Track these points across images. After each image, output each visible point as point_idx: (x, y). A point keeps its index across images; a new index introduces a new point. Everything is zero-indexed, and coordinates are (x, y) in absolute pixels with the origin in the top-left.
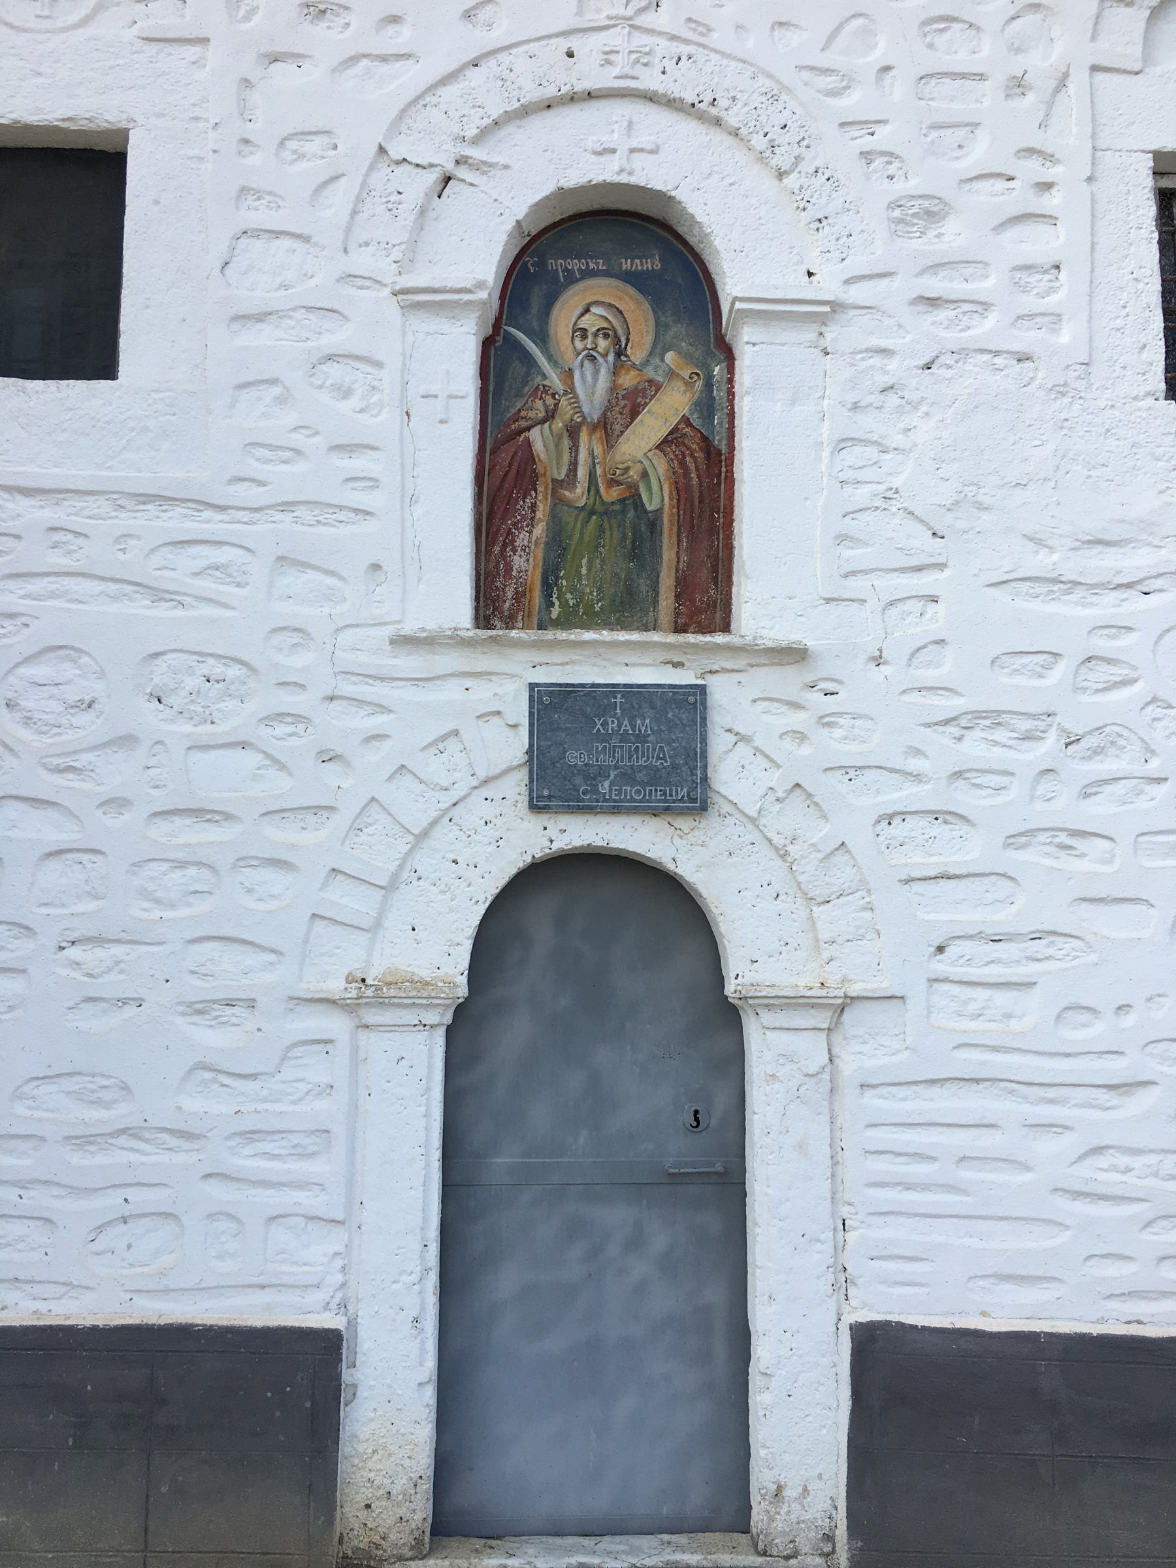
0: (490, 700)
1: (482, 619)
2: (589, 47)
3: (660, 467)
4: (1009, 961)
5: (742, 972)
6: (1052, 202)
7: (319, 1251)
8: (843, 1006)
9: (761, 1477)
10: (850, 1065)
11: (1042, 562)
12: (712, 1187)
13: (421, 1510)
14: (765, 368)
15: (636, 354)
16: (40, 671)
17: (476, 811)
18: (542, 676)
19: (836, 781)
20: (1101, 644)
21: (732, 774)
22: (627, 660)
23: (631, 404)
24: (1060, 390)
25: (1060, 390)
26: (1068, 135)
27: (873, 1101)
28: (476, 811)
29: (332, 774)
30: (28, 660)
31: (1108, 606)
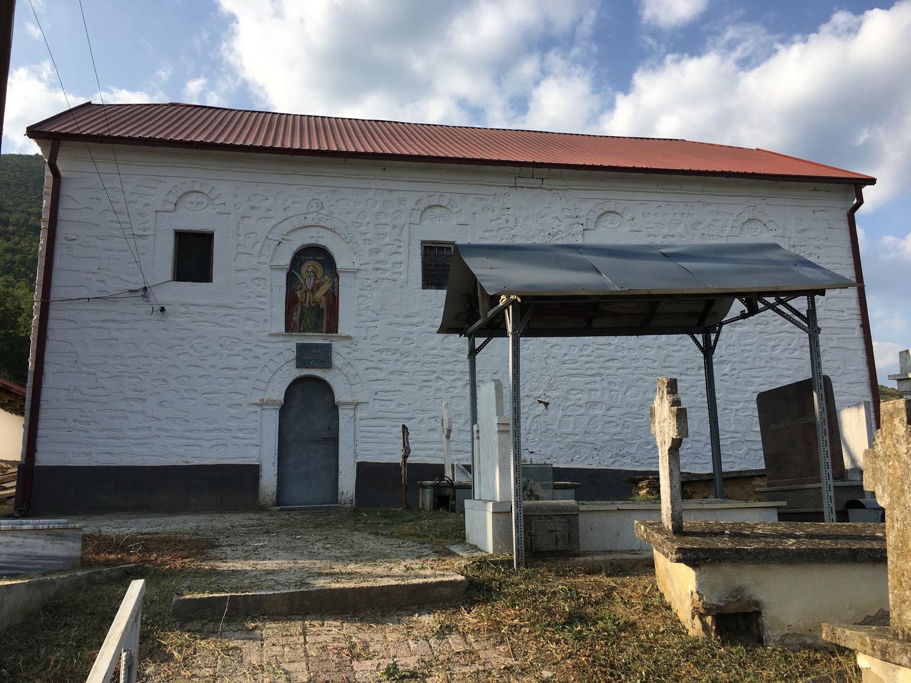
0: (289, 347)
1: (287, 331)
2: (309, 217)
3: (324, 299)
4: (389, 396)
5: (338, 399)
6: (401, 250)
7: (254, 451)
8: (357, 404)
9: (340, 491)
10: (358, 415)
11: (398, 320)
12: (332, 440)
13: (274, 498)
14: (345, 282)
15: (319, 276)
16: (197, 341)
17: (286, 368)
18: (298, 342)
19: (357, 362)
20: (408, 336)
21: (337, 361)
22: (316, 339)
23: (318, 286)
24: (401, 287)
25: (401, 287)
26: (405, 236)
27: (362, 422)
28: (286, 368)
29: (257, 361)
30: (196, 338)
31: (409, 329)
